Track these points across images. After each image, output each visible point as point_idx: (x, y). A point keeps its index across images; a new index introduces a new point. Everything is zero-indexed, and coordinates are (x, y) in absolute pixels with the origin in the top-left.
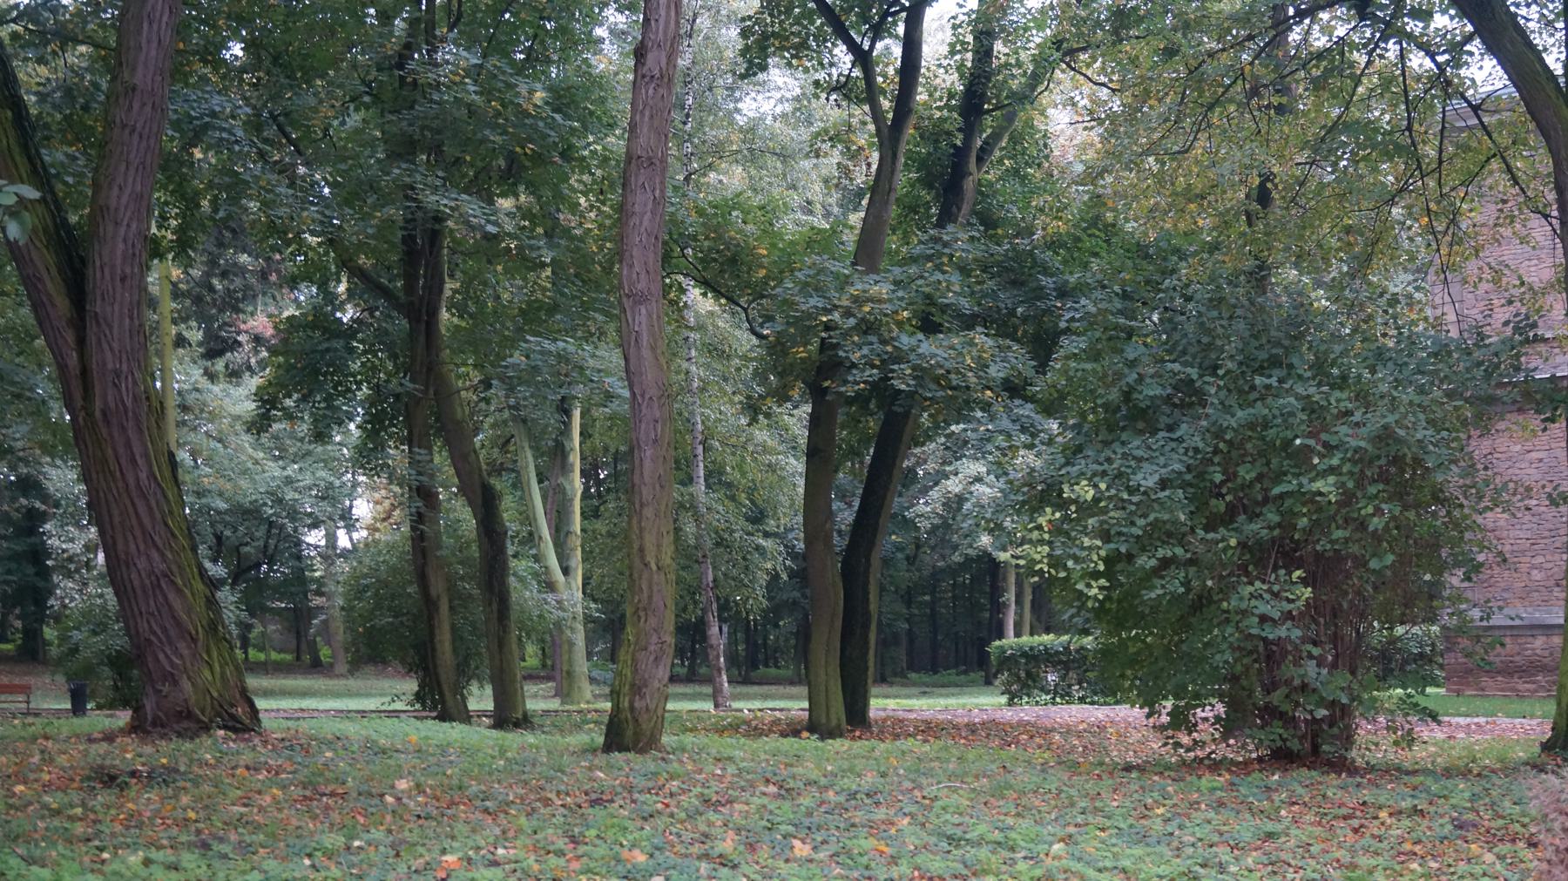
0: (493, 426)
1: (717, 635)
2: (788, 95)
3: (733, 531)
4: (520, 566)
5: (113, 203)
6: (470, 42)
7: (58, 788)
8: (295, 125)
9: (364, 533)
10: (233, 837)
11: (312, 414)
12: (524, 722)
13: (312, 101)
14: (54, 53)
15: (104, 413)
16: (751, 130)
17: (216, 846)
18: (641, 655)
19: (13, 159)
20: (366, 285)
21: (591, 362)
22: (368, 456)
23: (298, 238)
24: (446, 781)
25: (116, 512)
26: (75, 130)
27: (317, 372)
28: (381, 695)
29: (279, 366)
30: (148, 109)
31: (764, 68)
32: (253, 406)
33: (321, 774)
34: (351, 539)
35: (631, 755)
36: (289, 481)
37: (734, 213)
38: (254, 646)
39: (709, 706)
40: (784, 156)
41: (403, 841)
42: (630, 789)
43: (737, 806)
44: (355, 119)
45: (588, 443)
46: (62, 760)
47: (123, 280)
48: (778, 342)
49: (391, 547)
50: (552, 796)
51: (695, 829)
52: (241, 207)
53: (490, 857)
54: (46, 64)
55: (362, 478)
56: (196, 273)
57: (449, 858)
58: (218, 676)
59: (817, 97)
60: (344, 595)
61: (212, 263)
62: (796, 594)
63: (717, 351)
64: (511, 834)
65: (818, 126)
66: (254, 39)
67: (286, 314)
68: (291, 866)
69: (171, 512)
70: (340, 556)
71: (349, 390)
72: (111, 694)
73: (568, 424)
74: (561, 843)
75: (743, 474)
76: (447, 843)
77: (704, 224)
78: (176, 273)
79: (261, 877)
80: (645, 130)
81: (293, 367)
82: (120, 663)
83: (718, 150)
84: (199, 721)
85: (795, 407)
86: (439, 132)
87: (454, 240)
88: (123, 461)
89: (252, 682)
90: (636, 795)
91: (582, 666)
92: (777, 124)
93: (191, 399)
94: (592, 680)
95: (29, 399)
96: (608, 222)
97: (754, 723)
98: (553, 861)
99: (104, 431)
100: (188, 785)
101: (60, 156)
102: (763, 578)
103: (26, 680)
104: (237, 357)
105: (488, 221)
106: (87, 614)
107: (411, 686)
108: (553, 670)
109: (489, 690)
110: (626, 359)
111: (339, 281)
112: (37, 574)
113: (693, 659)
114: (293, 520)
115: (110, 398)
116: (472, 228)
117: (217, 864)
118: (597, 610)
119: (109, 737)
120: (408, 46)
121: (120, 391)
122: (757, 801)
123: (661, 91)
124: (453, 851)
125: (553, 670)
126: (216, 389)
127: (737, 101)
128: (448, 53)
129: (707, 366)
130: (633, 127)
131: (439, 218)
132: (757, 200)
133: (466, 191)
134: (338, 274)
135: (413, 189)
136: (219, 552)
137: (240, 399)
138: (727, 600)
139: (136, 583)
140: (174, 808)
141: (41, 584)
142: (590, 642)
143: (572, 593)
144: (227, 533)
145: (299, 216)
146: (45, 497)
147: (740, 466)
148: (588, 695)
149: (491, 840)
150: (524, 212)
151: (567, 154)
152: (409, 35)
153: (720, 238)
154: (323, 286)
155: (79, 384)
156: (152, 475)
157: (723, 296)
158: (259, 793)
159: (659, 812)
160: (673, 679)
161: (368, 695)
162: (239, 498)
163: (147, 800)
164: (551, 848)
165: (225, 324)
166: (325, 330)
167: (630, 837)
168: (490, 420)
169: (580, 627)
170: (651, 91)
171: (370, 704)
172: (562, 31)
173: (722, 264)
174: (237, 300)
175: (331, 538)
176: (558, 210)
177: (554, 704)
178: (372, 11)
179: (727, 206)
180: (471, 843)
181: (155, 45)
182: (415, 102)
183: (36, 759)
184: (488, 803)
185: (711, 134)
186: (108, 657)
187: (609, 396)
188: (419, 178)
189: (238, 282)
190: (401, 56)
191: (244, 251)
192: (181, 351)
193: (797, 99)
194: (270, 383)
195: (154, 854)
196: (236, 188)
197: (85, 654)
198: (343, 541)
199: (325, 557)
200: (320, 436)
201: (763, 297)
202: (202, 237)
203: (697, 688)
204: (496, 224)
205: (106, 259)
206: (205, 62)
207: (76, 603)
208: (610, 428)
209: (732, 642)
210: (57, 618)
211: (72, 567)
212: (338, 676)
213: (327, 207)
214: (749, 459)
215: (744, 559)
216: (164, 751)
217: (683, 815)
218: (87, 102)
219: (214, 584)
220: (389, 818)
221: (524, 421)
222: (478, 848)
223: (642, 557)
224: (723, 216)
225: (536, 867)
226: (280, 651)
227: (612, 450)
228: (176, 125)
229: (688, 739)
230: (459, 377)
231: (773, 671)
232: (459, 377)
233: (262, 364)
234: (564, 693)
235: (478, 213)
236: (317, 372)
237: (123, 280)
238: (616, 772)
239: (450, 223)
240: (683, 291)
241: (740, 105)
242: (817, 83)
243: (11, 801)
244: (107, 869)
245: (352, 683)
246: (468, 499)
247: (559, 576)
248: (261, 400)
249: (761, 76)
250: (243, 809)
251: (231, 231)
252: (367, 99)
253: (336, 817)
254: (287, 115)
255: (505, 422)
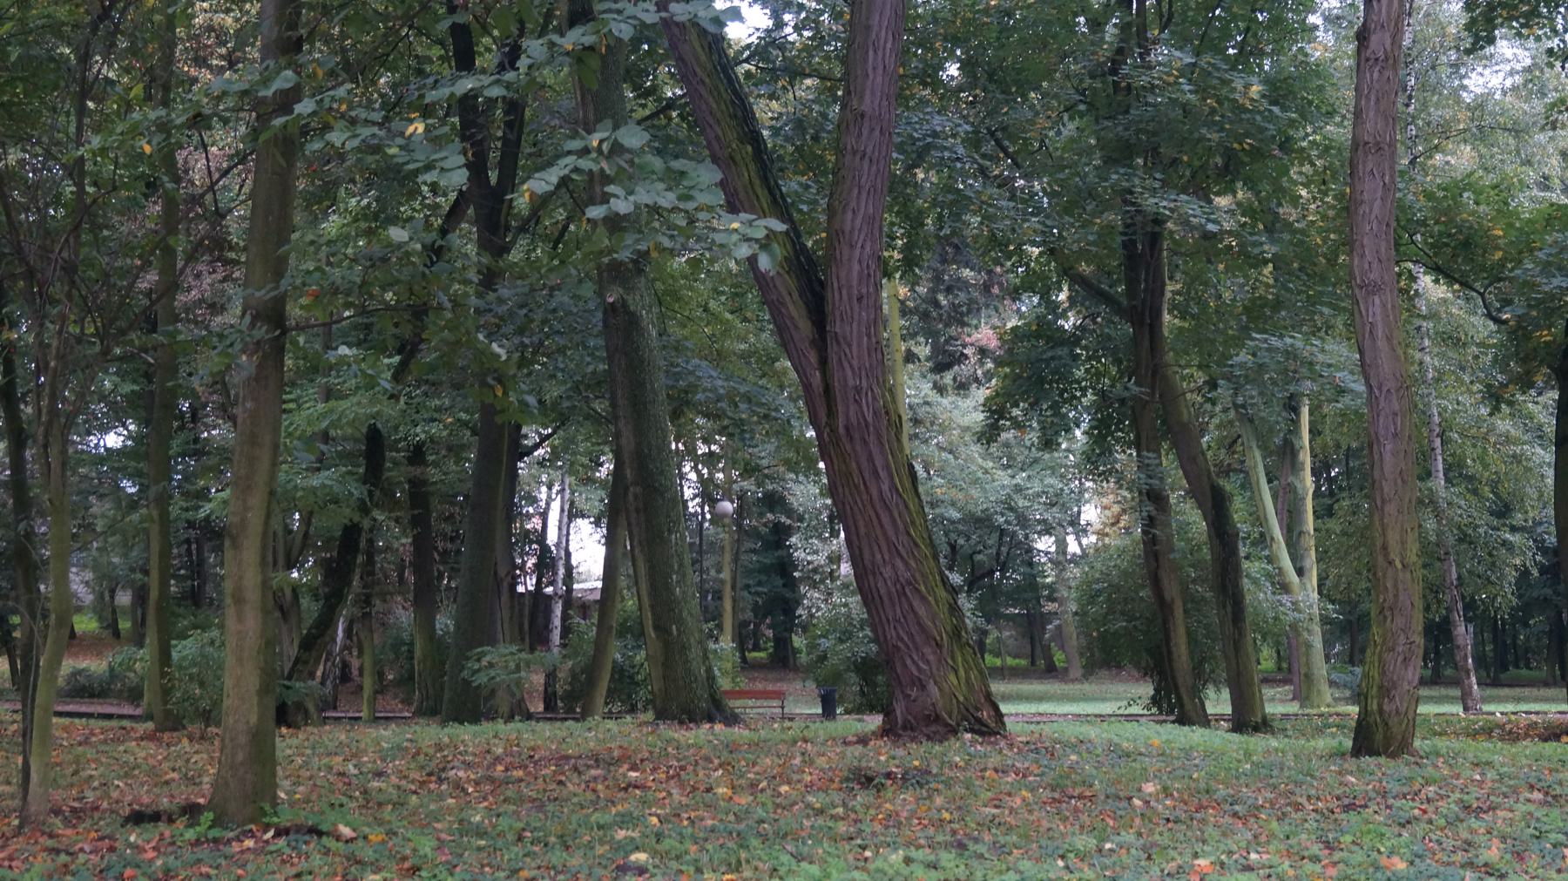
0: (1218, 427)
1: (1463, 633)
2: (1518, 67)
3: (1477, 526)
4: (1253, 567)
5: (847, 228)
6: (1182, 42)
7: (819, 789)
8: (1013, 139)
9: (1093, 539)
10: (987, 838)
11: (1039, 422)
12: (1265, 726)
13: (1030, 115)
14: (784, 87)
15: (847, 428)
16: (1480, 105)
17: (972, 846)
18: (1388, 657)
19: (755, 192)
20: (1088, 292)
21: (1321, 357)
22: (1096, 460)
23: (1019, 250)
24: (1193, 785)
25: (861, 524)
26: (808, 161)
27: (1042, 381)
28: (1117, 699)
29: (1006, 376)
30: (877, 133)
31: (1491, 41)
32: (981, 416)
33: (1068, 777)
34: (1080, 544)
35: (1382, 760)
36: (1018, 489)
37: (1466, 195)
38: (991, 652)
39: (1458, 709)
40: (1517, 131)
41: (1154, 845)
42: (1384, 794)
43: (1501, 814)
44: (1070, 128)
45: (1319, 440)
46: (821, 762)
47: (860, 299)
48: (1519, 326)
49: (1122, 552)
50: (1303, 801)
51: (1456, 837)
52: (964, 223)
53: (1243, 861)
54: (777, 99)
55: (1089, 484)
56: (922, 290)
57: (1202, 862)
58: (963, 681)
59: (1551, 66)
60: (1078, 600)
61: (937, 279)
62: (1548, 591)
63: (1452, 339)
64: (1263, 839)
65: (1552, 97)
66: (970, 57)
67: (1009, 325)
68: (1046, 866)
69: (913, 523)
70: (1070, 562)
71: (1075, 397)
72: (858, 699)
73: (1296, 423)
74: (1316, 849)
75: (1486, 466)
76: (1198, 847)
77: (1433, 208)
78: (903, 291)
79: (1018, 877)
80: (1372, 114)
81: (1019, 376)
82: (865, 669)
83: (1445, 130)
84: (947, 725)
85: (1540, 394)
86: (1155, 134)
87: (1175, 241)
88: (867, 475)
89: (997, 687)
90: (1391, 801)
91: (1321, 668)
92: (1508, 99)
93: (922, 412)
94: (1332, 683)
95: (776, 419)
96: (1331, 213)
97: (1508, 727)
98: (1309, 867)
99: (848, 447)
100: (941, 787)
101: (794, 186)
102: (1512, 575)
103: (778, 686)
104: (964, 370)
105: (1208, 220)
106: (832, 622)
107: (1147, 690)
108: (1290, 672)
109: (1226, 694)
110: (1361, 352)
111: (1061, 290)
112: (784, 585)
113: (1437, 660)
114: (1024, 527)
115: (852, 413)
116: (1193, 228)
117: (974, 863)
118: (1335, 611)
119: (863, 740)
120: (1120, 51)
121: (860, 406)
122: (1522, 808)
123: (1387, 73)
124: (1205, 855)
125: (1290, 672)
126: (945, 401)
127: (1462, 77)
128: (1161, 54)
129: (1442, 356)
130: (1358, 114)
131: (1158, 221)
132: (1489, 179)
133: (1184, 191)
134: (1059, 283)
135: (1131, 193)
136: (953, 560)
137: (968, 410)
138: (1472, 598)
139: (882, 592)
140: (929, 809)
141: (788, 595)
142: (1328, 644)
143: (1307, 594)
144: (961, 541)
145: (1021, 227)
146: (790, 512)
147: (1481, 459)
148: (1329, 699)
149: (1243, 844)
150: (1246, 209)
151: (1286, 145)
152: (1122, 40)
153: (1451, 220)
154: (1045, 296)
155: (823, 402)
156: (893, 487)
157: (1457, 281)
158: (1009, 795)
159: (1416, 819)
160: (1423, 682)
161: (1104, 700)
162: (971, 507)
163: (902, 801)
164: (1306, 854)
165: (951, 338)
166: (1049, 339)
167: (1388, 844)
168: (1216, 421)
169: (1317, 629)
170: (1376, 75)
171: (1107, 708)
172: (1276, 22)
173: (1454, 248)
174: (962, 314)
175: (1062, 545)
176: (1280, 204)
177: (1293, 708)
178: (1082, 19)
179: (1457, 188)
180: (1222, 847)
181: (880, 71)
182: (1129, 107)
183: (797, 761)
184: (1237, 808)
185: (1436, 114)
186: (855, 662)
187: (1341, 391)
188: (1137, 181)
189: (962, 297)
190: (1113, 62)
191: (967, 266)
192: (911, 366)
193: (1528, 70)
194: (998, 394)
195: (913, 853)
196: (959, 203)
197: (833, 660)
198: (1073, 547)
199: (1056, 563)
200: (1048, 444)
201: (1500, 280)
202: (927, 256)
203: (1443, 691)
204: (1215, 222)
205: (843, 282)
206: (925, 85)
207: (822, 612)
208: (1341, 424)
209: (1478, 643)
210: (805, 628)
211: (817, 577)
212: (1073, 681)
213: (1047, 217)
214: (1491, 450)
215: (1490, 554)
216: (916, 754)
217: (1442, 822)
218: (817, 132)
219: (954, 591)
220: (1138, 821)
221: (1251, 421)
222: (1230, 853)
223: (1386, 555)
224: (1453, 198)
225: (1291, 872)
226: (1015, 657)
227: (1344, 447)
228: (900, 148)
229: (1442, 744)
230: (1183, 378)
231: (1524, 672)
232: (1183, 378)
233: (989, 375)
234: (1303, 695)
235: (1198, 212)
236: (1042, 381)
237: (860, 299)
238: (1368, 777)
239: (1169, 225)
240: (1414, 279)
241: (1466, 82)
242: (1550, 52)
243: (778, 801)
244: (871, 866)
245: (1087, 687)
246: (1197, 501)
247: (1293, 577)
248: (990, 410)
249: (1489, 50)
250: (995, 811)
251: (954, 248)
252: (1082, 107)
253: (1085, 818)
254: (1004, 129)
255: (1231, 422)
